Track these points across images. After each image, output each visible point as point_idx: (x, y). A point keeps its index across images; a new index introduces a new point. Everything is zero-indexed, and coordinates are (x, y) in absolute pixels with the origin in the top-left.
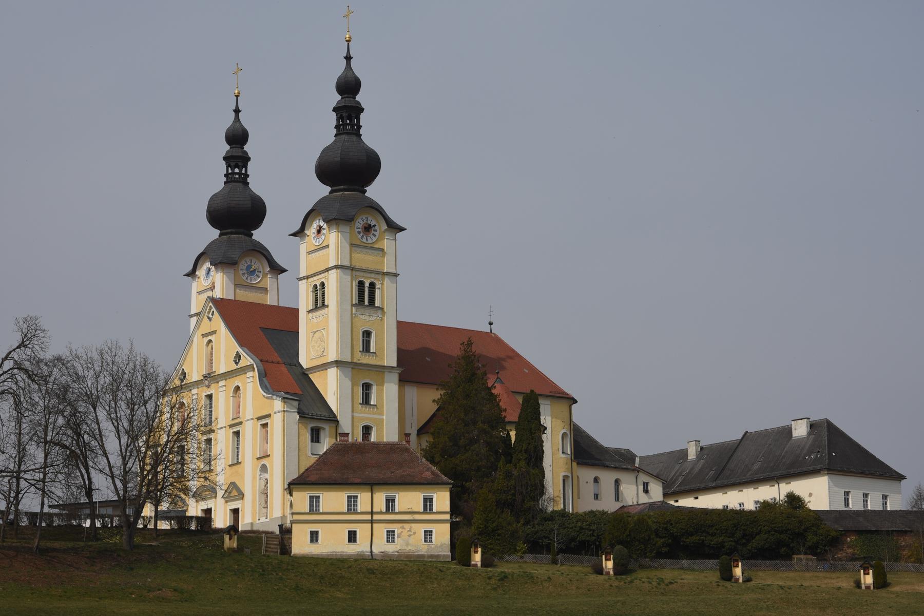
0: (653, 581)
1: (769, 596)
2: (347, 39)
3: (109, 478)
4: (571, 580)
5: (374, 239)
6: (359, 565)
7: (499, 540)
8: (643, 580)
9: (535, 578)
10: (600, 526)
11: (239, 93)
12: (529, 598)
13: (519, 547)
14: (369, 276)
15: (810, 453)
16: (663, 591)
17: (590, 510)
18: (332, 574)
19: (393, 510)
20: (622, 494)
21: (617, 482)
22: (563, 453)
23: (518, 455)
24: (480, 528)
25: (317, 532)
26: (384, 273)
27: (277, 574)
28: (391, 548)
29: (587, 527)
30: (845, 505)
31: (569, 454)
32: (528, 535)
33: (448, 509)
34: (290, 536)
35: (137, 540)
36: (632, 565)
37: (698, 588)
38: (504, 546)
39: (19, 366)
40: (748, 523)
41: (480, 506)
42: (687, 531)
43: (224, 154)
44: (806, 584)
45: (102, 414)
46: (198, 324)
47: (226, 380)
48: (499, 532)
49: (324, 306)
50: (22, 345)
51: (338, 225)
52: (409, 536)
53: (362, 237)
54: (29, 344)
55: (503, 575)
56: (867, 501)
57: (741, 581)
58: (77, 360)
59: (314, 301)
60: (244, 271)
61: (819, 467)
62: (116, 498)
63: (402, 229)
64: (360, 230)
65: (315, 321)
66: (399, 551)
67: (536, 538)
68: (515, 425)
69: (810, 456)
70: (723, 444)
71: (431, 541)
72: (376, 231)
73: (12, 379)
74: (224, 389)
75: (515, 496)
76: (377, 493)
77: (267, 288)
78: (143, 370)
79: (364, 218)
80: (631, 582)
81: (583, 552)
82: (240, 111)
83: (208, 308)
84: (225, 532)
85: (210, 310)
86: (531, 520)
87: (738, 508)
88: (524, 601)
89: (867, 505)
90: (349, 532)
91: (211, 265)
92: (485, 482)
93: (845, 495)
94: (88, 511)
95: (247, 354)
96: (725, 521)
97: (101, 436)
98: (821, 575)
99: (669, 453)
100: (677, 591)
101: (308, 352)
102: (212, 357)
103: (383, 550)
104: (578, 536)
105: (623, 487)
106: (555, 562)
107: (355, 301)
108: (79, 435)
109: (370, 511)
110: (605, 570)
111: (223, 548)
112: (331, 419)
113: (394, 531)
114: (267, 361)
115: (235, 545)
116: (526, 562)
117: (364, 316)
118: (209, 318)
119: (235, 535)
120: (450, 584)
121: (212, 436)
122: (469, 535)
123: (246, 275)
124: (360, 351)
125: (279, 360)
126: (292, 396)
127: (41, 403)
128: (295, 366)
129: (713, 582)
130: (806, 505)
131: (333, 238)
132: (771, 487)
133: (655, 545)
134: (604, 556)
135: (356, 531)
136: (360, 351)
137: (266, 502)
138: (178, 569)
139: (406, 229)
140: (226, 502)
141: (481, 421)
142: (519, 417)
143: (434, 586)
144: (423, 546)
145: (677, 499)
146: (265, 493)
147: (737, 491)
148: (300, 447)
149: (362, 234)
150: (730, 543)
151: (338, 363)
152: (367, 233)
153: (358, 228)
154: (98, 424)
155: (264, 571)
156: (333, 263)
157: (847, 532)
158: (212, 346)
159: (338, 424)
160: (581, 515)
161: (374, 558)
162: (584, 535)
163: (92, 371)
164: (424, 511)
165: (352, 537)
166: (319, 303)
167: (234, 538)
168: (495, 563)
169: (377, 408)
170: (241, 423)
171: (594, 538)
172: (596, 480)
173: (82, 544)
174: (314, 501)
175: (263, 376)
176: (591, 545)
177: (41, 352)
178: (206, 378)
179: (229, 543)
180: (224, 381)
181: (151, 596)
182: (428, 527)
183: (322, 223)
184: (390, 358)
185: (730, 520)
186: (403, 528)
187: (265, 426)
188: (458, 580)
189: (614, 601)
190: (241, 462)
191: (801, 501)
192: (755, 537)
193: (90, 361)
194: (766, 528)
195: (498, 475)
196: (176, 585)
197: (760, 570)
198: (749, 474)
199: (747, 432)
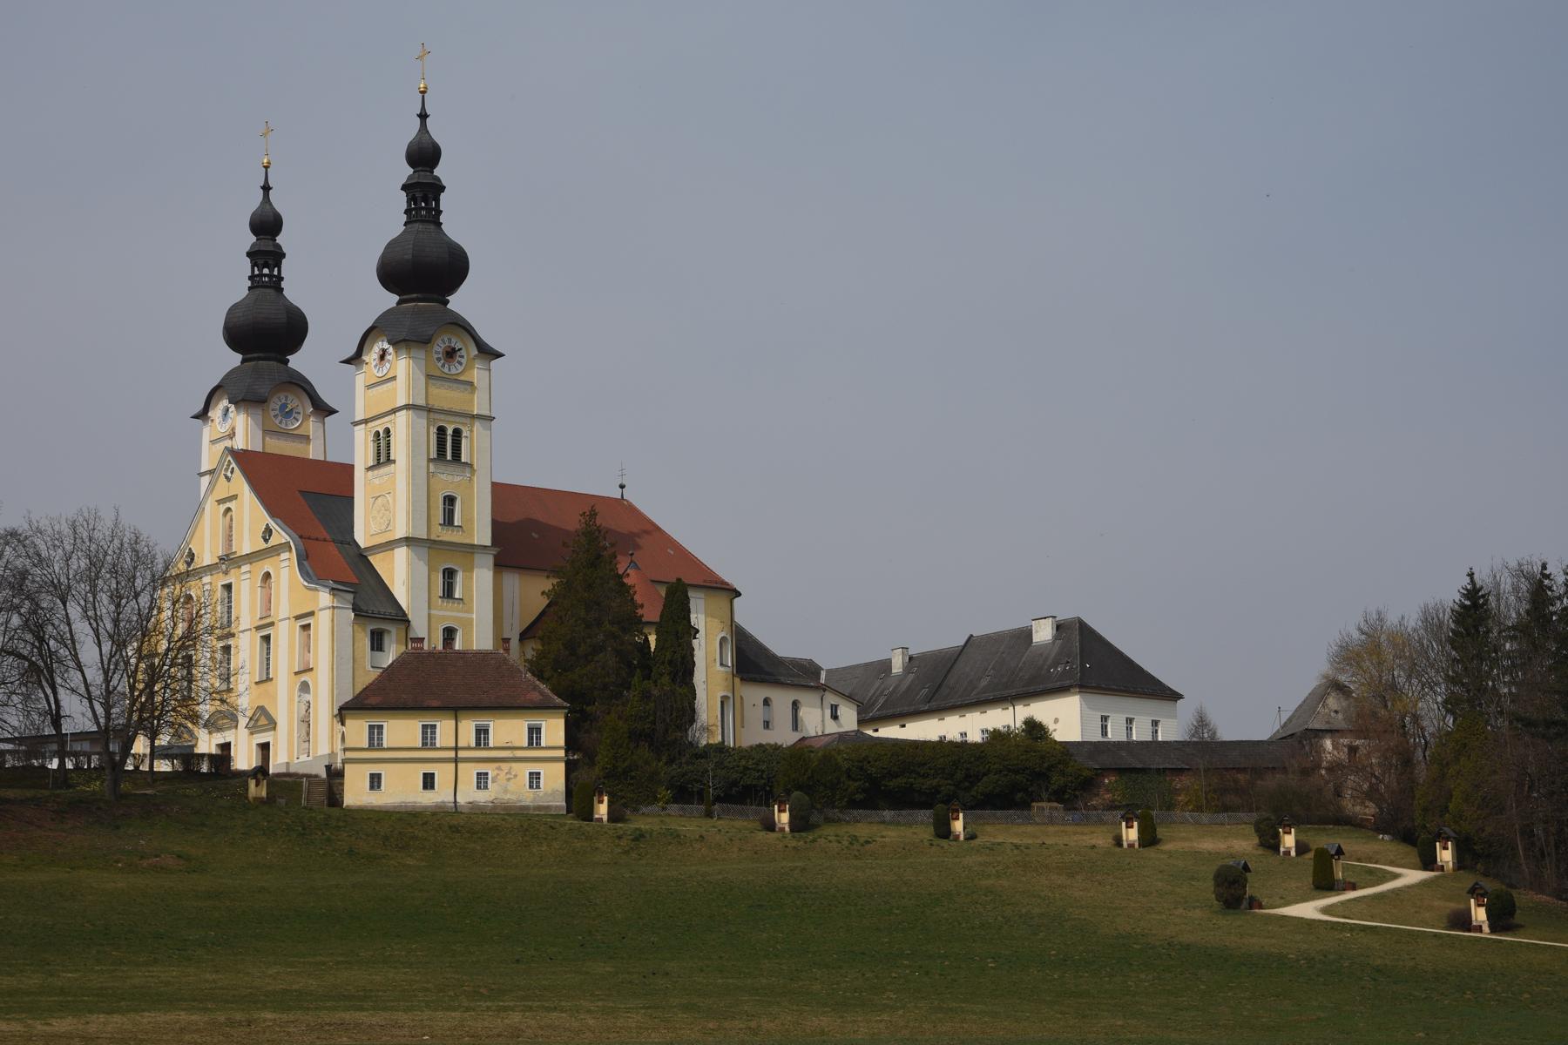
1: (999, 859)
4: (731, 840)
5: (460, 369)
11: (426, 88)
15: (1055, 664)
16: (857, 854)
17: (757, 743)
19: (486, 744)
21: (795, 705)
25: (379, 776)
26: (473, 415)
27: (323, 834)
28: (482, 797)
32: (672, 778)
33: (562, 743)
35: (125, 787)
40: (973, 759)
43: (248, 249)
45: (74, 611)
46: (212, 485)
47: (251, 563)
48: (633, 774)
49: (389, 461)
51: (408, 348)
52: (509, 779)
53: (443, 366)
55: (638, 832)
56: (1131, 728)
57: (962, 838)
60: (277, 412)
61: (1067, 683)
62: (95, 728)
64: (440, 356)
65: (377, 481)
69: (1056, 668)
70: (940, 651)
71: (538, 787)
74: (248, 576)
76: (463, 722)
78: (134, 550)
79: (446, 339)
80: (814, 841)
81: (748, 801)
87: (958, 739)
89: (1131, 734)
91: (230, 403)
94: (55, 747)
97: (73, 642)
98: (1070, 829)
99: (866, 665)
101: (367, 525)
102: (232, 531)
103: (471, 800)
105: (802, 713)
106: (709, 815)
107: (434, 455)
108: (41, 640)
110: (778, 826)
111: (247, 798)
113: (487, 774)
114: (309, 538)
115: (264, 794)
118: (227, 477)
123: (280, 418)
126: (344, 586)
128: (349, 544)
129: (925, 840)
131: (402, 366)
134: (776, 806)
135: (433, 774)
137: (308, 734)
140: (252, 734)
142: (661, 616)
146: (306, 721)
149: (442, 362)
151: (408, 541)
152: (450, 360)
153: (437, 353)
154: (69, 624)
155: (304, 829)
156: (401, 401)
157: (1105, 771)
165: (429, 782)
166: (383, 457)
167: (263, 785)
170: (272, 624)
171: (763, 781)
172: (767, 702)
173: (46, 793)
174: (375, 732)
175: (304, 558)
179: (255, 790)
182: (535, 768)
183: (386, 346)
184: (482, 534)
186: (499, 769)
187: (306, 627)
188: (576, 841)
190: (272, 679)
193: (57, 536)
199: (972, 636)
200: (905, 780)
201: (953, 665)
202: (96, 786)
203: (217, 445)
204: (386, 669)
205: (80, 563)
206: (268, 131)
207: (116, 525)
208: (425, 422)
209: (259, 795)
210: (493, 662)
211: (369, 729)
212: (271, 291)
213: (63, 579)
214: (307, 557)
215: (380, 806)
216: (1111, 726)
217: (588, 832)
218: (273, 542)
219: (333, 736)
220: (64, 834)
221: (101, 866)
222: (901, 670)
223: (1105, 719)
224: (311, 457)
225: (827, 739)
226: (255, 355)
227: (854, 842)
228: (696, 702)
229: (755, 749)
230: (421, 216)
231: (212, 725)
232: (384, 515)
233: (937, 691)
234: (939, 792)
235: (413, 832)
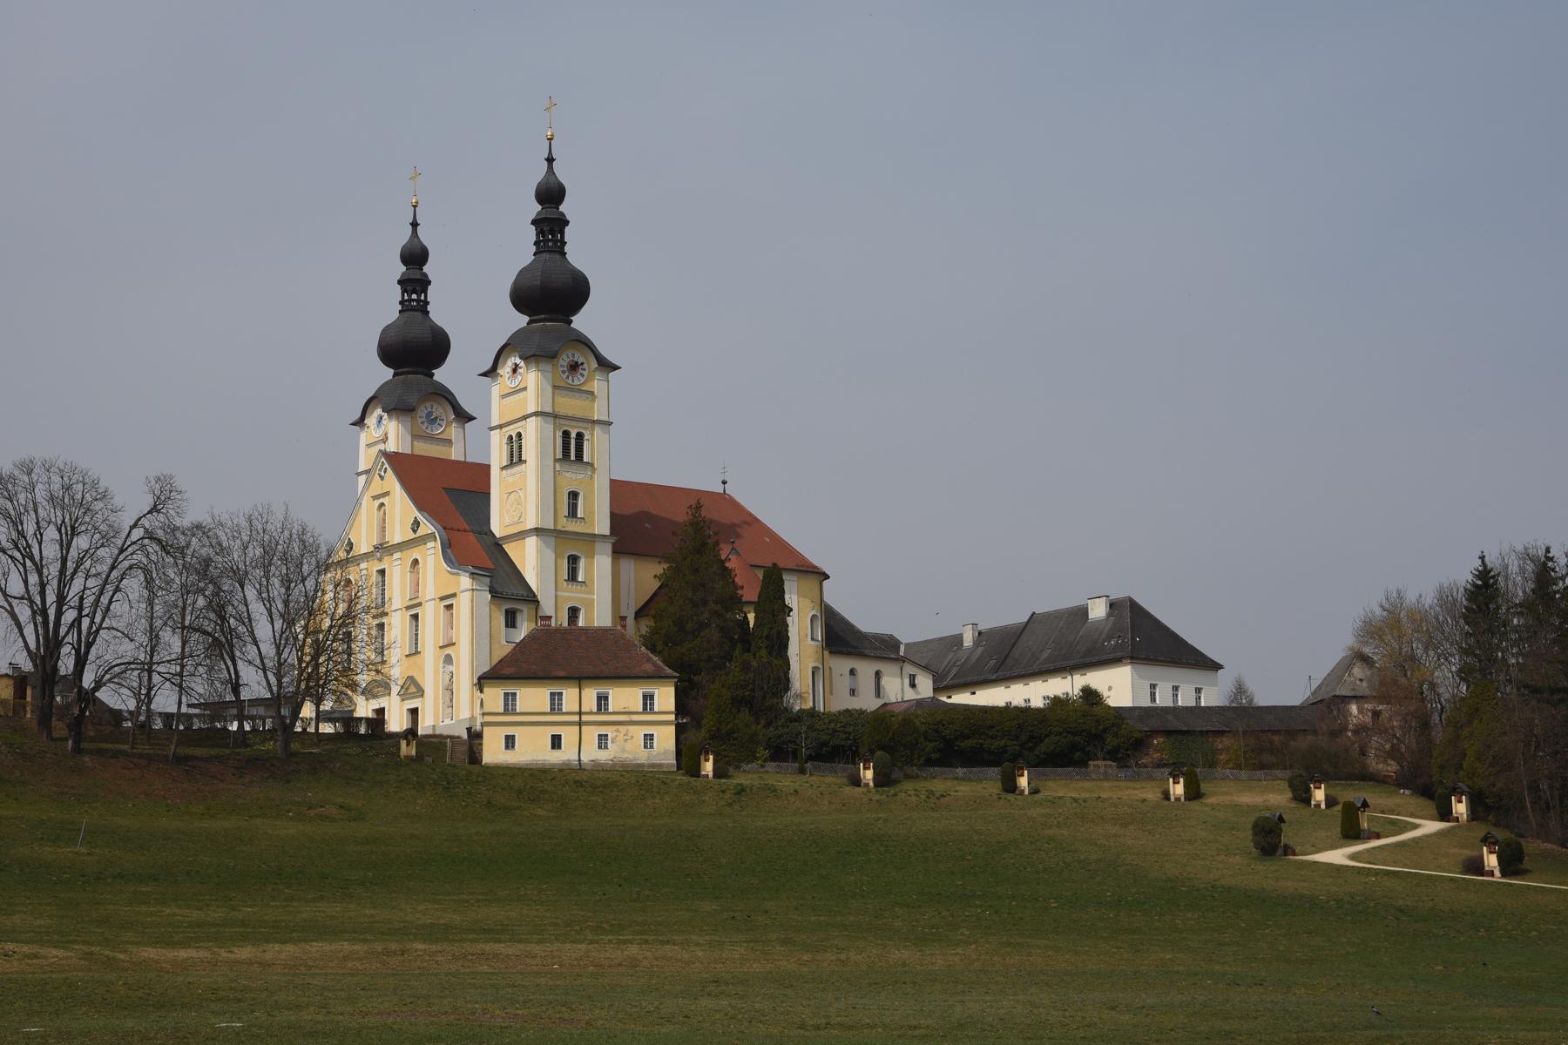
1: (1060, 811)
7: (735, 745)
15: (1109, 638)
21: (878, 675)
27: (465, 788)
28: (603, 756)
32: (770, 739)
33: (673, 708)
35: (295, 746)
39: (150, 535)
44: (1104, 795)
45: (251, 593)
46: (368, 484)
47: (401, 551)
48: (735, 735)
49: (521, 461)
50: (154, 509)
51: (537, 363)
52: (626, 740)
53: (568, 377)
55: (739, 787)
56: (1177, 695)
57: (1026, 792)
60: (424, 419)
61: (1119, 655)
63: (616, 368)
64: (565, 369)
65: (510, 479)
71: (652, 747)
74: (399, 562)
77: (451, 440)
79: (570, 354)
85: (382, 466)
89: (1177, 700)
94: (234, 711)
97: (250, 620)
99: (941, 639)
101: (501, 517)
105: (886, 681)
106: (802, 771)
107: (559, 455)
108: (223, 619)
110: (864, 781)
111: (399, 756)
115: (414, 752)
121: (385, 620)
123: (426, 424)
127: (177, 580)
131: (532, 377)
134: (861, 764)
135: (560, 735)
137: (451, 701)
139: (619, 368)
140: (403, 700)
145: (973, 691)
146: (449, 689)
151: (538, 531)
154: (247, 605)
155: (448, 783)
158: (385, 511)
165: (556, 742)
166: (515, 458)
168: (730, 774)
171: (849, 742)
172: (852, 672)
173: (228, 751)
174: (510, 698)
175: (447, 546)
177: (177, 519)
183: (518, 361)
184: (602, 525)
186: (617, 731)
187: (450, 607)
188: (685, 794)
198: (1036, 664)
199: (1034, 613)
200: (975, 741)
202: (270, 745)
205: (255, 552)
207: (286, 518)
213: (241, 566)
214: (450, 546)
218: (421, 532)
219: (473, 703)
220: (244, 787)
223: (1153, 686)
224: (453, 458)
225: (906, 704)
227: (931, 796)
231: (369, 693)
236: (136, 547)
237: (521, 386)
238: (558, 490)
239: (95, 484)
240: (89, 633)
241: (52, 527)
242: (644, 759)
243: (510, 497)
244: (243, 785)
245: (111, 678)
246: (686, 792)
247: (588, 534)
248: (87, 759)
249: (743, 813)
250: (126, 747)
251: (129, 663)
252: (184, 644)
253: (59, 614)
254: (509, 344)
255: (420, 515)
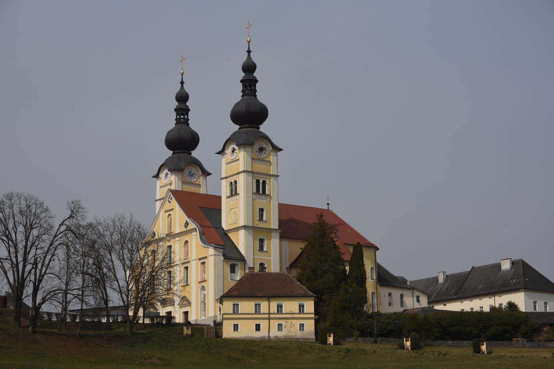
0: (435, 353)
1: (505, 362)
2: (248, 41)
3: (119, 294)
4: (387, 353)
5: (265, 155)
6: (263, 344)
7: (343, 329)
8: (429, 352)
9: (366, 352)
10: (400, 321)
11: (183, 72)
12: (364, 363)
13: (354, 333)
14: (258, 176)
15: (512, 280)
16: (442, 359)
17: (394, 312)
18: (248, 349)
19: (282, 312)
20: (405, 302)
21: (402, 296)
22: (372, 279)
23: (351, 280)
24: (332, 322)
25: (237, 325)
26: (271, 175)
27: (217, 349)
28: (280, 334)
29: (392, 322)
30: (534, 309)
31: (374, 279)
32: (358, 326)
33: (313, 311)
34: (221, 327)
35: (134, 330)
36: (422, 343)
37: (462, 358)
38: (346, 332)
39: (69, 229)
40: (486, 319)
41: (332, 309)
42: (451, 324)
43: (175, 108)
44: (525, 355)
45: (114, 257)
46: (162, 206)
47: (180, 237)
48: (343, 324)
49: (236, 194)
50: (71, 217)
51: (244, 147)
52: (291, 327)
53: (258, 154)
54: (75, 216)
55: (347, 349)
56: (546, 307)
57: (486, 353)
58: (100, 225)
59: (231, 191)
60: (187, 175)
61: (518, 287)
62: (122, 304)
63: (281, 150)
64: (257, 150)
65: (231, 203)
66: (285, 336)
67: (363, 328)
68: (349, 263)
69: (512, 281)
70: (459, 273)
71: (303, 330)
72: (266, 151)
73: (65, 236)
74: (178, 242)
75: (351, 304)
76: (272, 302)
77: (200, 184)
78: (138, 231)
79: (259, 143)
80: (423, 354)
81: (390, 336)
82: (184, 83)
83: (169, 196)
84: (184, 325)
85: (170, 197)
86: (360, 317)
87: (469, 310)
88: (362, 365)
89: (547, 309)
90: (256, 325)
91: (168, 171)
92: (333, 296)
93: (534, 303)
94: (104, 313)
95: (192, 222)
96: (473, 318)
97: (114, 270)
98: (532, 350)
99: (427, 279)
100: (450, 359)
101: (227, 221)
102: (171, 224)
103: (276, 335)
104: (387, 327)
105: (405, 299)
106: (375, 342)
107: (255, 191)
108: (101, 269)
109: (268, 312)
110: (406, 347)
111: (183, 334)
112: (242, 259)
113: (282, 324)
114: (204, 226)
115: (190, 333)
116: (359, 342)
117: (259, 200)
118: (169, 201)
119: (189, 327)
120: (317, 355)
121: (172, 270)
122: (325, 326)
123: (188, 177)
124: (258, 220)
125: (210, 225)
126: (219, 246)
127: (81, 250)
128: (220, 229)
129: (470, 354)
130: (519, 309)
131: (242, 154)
132: (499, 297)
133: (434, 332)
134: (405, 339)
135: (238, 324)
136: (258, 220)
137: (205, 308)
138: (159, 346)
139: (283, 150)
140: (181, 307)
141: (330, 260)
142: (352, 258)
143: (308, 356)
144: (299, 333)
145: (445, 304)
146: (204, 302)
147: (460, 302)
148: (224, 275)
149: (258, 153)
150: (476, 331)
151: (245, 227)
152: (261, 152)
153: (256, 149)
154: (112, 262)
155: (209, 347)
156: (242, 169)
157: (544, 325)
158: (171, 217)
159: (246, 262)
160: (389, 315)
161: (271, 340)
162: (390, 326)
163: (108, 232)
164: (299, 312)
165: (258, 327)
166: (234, 192)
167: (189, 328)
168: (341, 343)
169: (268, 253)
170: (189, 262)
171: (397, 328)
172: (390, 295)
173: (104, 332)
174: (236, 306)
175: (202, 235)
176: (395, 332)
177: (82, 221)
178: (167, 236)
179: (187, 331)
180: (179, 237)
181: (147, 362)
182: (302, 322)
183: (235, 146)
184: (275, 225)
185: (476, 318)
186: (287, 322)
187: (203, 263)
188: (321, 353)
189: (414, 365)
190: (189, 285)
191: (517, 306)
192: (491, 328)
193: (107, 226)
194: (497, 322)
195: (340, 291)
196: (160, 356)
197: (496, 347)
198: (476, 291)
199: (474, 267)
200: (457, 328)
201: (466, 279)
202: (122, 329)
203: (163, 188)
204: (239, 281)
205: (116, 237)
206: (249, 26)
207: (131, 221)
208: (251, 178)
209: (188, 333)
210: (283, 277)
211: (233, 305)
212: (184, 125)
213: (110, 243)
214: (204, 234)
215: (238, 338)
216: (538, 305)
217: (326, 349)
218: (189, 228)
219: (215, 309)
220: (112, 349)
221: (129, 363)
222: (443, 281)
223: (535, 302)
224: (201, 193)
225: (416, 310)
226: (178, 151)
227: (440, 354)
228: (367, 294)
229: (393, 314)
230: (181, 121)
231: (164, 303)
232: (234, 216)
233: (460, 290)
234: (472, 334)
235: (253, 349)
236: (61, 235)
237: (236, 159)
238: (254, 207)
239: (41, 205)
240: (40, 276)
241: (21, 225)
242: (299, 335)
243: (231, 211)
244: (112, 348)
245: (51, 297)
246: (321, 352)
247: (268, 228)
248: (38, 336)
249: (351, 362)
250: (56, 330)
251: (56, 290)
252: (84, 281)
253: (24, 266)
254: (230, 139)
255: (188, 219)
